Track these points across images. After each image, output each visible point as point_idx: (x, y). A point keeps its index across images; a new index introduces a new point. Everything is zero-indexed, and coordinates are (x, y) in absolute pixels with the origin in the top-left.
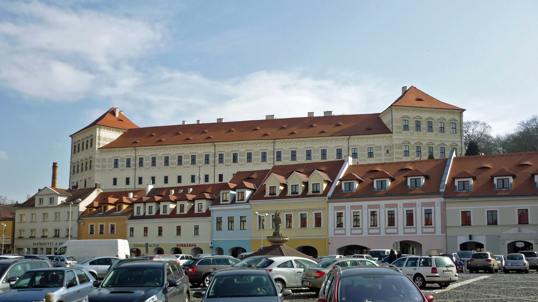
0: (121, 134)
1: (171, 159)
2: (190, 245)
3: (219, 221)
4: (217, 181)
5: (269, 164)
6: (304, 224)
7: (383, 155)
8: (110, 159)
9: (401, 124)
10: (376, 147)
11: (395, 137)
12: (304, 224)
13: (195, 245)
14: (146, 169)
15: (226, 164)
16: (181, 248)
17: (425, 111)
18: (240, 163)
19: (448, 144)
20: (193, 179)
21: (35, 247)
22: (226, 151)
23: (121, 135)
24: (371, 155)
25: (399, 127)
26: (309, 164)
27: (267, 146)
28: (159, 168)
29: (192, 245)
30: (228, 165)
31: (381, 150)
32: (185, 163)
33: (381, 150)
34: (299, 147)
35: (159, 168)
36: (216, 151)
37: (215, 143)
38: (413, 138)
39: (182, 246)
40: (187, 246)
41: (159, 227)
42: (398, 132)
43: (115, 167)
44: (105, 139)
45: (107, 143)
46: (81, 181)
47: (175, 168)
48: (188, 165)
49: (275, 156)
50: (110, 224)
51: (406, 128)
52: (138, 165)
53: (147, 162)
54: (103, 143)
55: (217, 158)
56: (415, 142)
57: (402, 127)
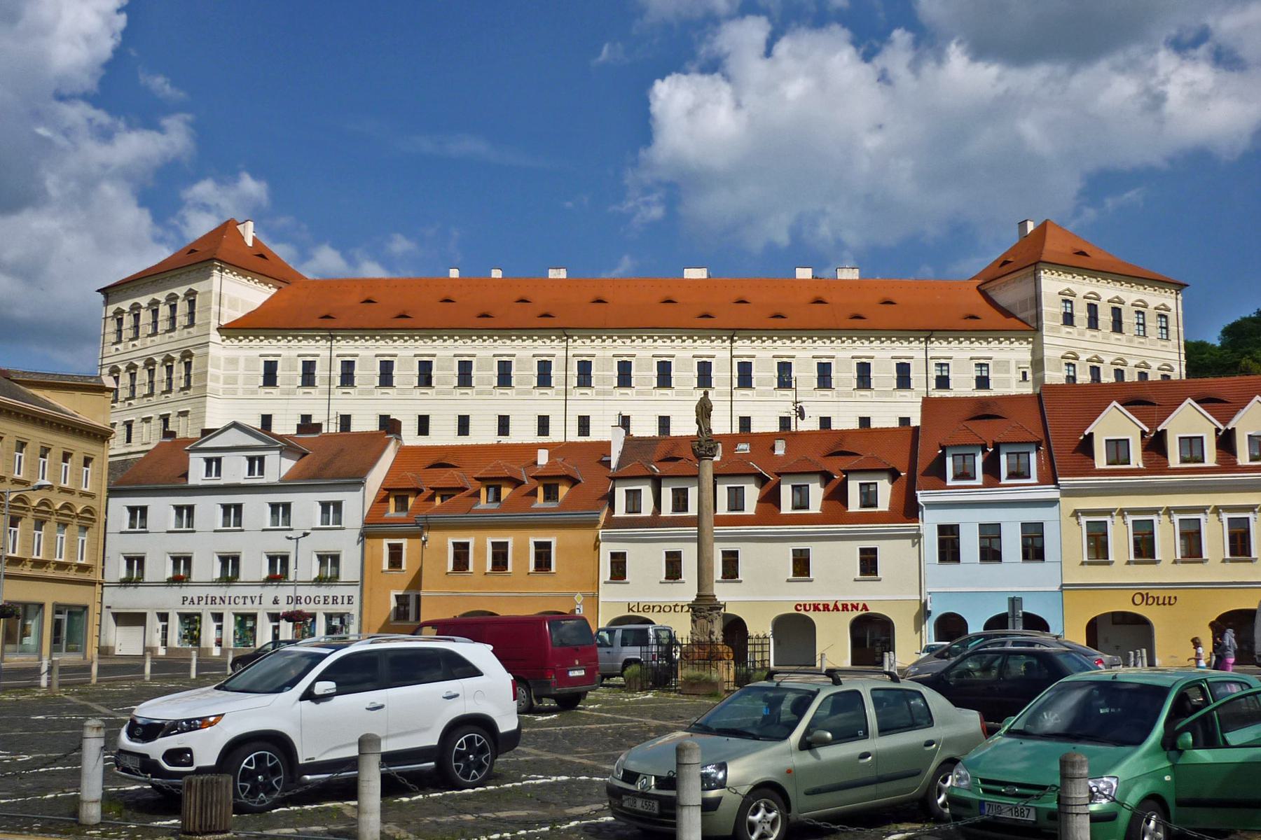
0: (274, 290)
2: (845, 607)
4: (573, 436)
7: (1014, 383)
8: (248, 360)
9: (1060, 310)
10: (997, 363)
11: (1046, 340)
13: (865, 607)
14: (639, 393)
16: (811, 614)
17: (1006, 284)
19: (1108, 359)
20: (543, 424)
21: (189, 609)
23: (273, 296)
24: (983, 382)
25: (1054, 316)
26: (941, 399)
28: (403, 391)
29: (855, 607)
30: (604, 393)
31: (1008, 371)
32: (481, 382)
33: (1008, 371)
34: (840, 354)
35: (403, 391)
36: (570, 353)
38: (1084, 345)
39: (816, 608)
42: (1052, 329)
44: (233, 305)
45: (239, 314)
46: (147, 420)
49: (736, 373)
50: (450, 542)
51: (1068, 319)
52: (338, 381)
54: (231, 315)
55: (574, 371)
56: (1089, 356)
57: (1061, 318)
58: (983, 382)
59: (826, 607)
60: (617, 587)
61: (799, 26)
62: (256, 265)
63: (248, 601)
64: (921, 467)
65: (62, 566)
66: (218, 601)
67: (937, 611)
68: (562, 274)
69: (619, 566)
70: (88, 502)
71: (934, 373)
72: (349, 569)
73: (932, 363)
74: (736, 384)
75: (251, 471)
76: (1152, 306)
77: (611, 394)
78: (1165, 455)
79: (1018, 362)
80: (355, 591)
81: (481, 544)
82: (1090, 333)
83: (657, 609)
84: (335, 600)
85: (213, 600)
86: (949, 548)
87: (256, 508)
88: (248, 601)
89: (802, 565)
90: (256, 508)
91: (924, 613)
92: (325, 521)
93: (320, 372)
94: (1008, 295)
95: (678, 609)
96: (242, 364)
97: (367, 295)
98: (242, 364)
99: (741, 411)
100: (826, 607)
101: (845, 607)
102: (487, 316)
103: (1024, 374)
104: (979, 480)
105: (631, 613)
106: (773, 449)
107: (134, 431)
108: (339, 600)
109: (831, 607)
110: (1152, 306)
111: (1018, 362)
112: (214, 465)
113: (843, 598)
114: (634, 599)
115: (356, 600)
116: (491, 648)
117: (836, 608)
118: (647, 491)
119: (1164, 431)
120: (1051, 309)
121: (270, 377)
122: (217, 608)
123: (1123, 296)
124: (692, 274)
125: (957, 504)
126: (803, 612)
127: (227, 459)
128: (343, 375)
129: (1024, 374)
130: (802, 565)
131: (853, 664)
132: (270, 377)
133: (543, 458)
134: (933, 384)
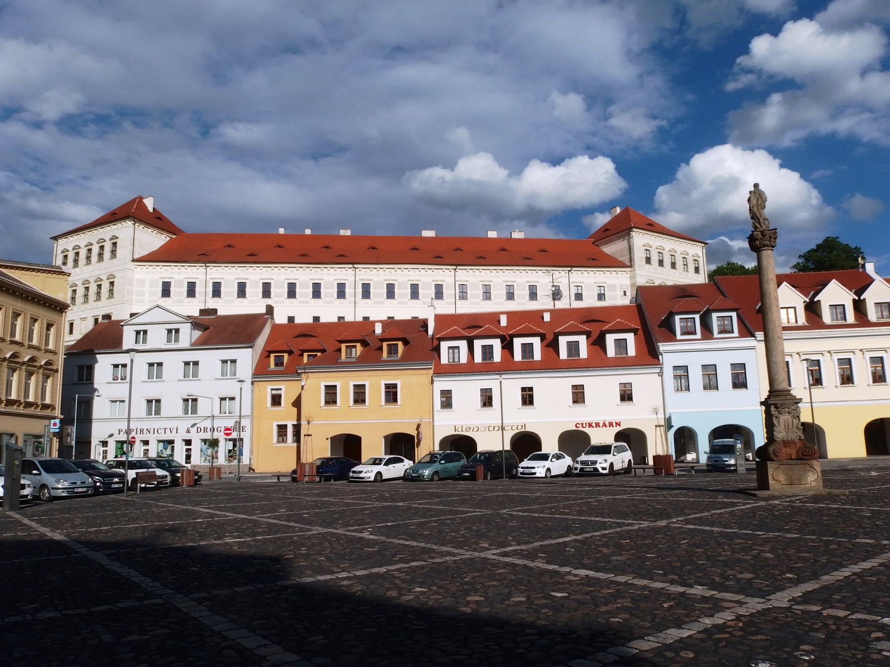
1: (276, 287)
2: (611, 424)
3: (682, 374)
5: (448, 303)
6: (847, 379)
7: (619, 298)
10: (609, 286)
11: (637, 272)
12: (847, 379)
15: (376, 300)
16: (587, 430)
18: (376, 300)
22: (176, 277)
24: (601, 297)
27: (445, 275)
30: (378, 303)
34: (375, 279)
37: (356, 266)
39: (590, 425)
40: (604, 425)
41: (523, 389)
43: (239, 297)
46: (83, 319)
47: (308, 302)
48: (308, 299)
49: (457, 291)
51: (648, 260)
53: (401, 291)
55: (359, 290)
58: (601, 297)
59: (597, 425)
60: (447, 412)
62: (156, 221)
63: (168, 431)
64: (653, 325)
65: (29, 405)
66: (145, 431)
67: (677, 424)
68: (348, 233)
69: (447, 400)
70: (50, 356)
71: (574, 291)
73: (572, 285)
74: (457, 297)
75: (169, 340)
76: (690, 255)
78: (820, 317)
79: (621, 285)
81: (345, 383)
82: (660, 268)
83: (476, 429)
85: (142, 431)
87: (173, 363)
88: (168, 431)
89: (578, 395)
90: (173, 363)
91: (669, 424)
92: (149, 412)
93: (348, 291)
94: (610, 249)
95: (491, 429)
96: (147, 283)
97: (227, 243)
98: (147, 283)
100: (597, 425)
101: (611, 424)
103: (625, 292)
104: (699, 335)
105: (457, 433)
106: (543, 318)
107: (75, 326)
109: (601, 425)
110: (690, 255)
111: (621, 285)
112: (142, 335)
113: (608, 419)
114: (459, 423)
117: (604, 425)
118: (463, 345)
119: (819, 301)
120: (639, 255)
121: (166, 291)
122: (145, 437)
123: (676, 248)
124: (426, 234)
125: (681, 352)
126: (581, 429)
128: (214, 291)
129: (625, 292)
130: (578, 395)
131: (870, 451)
132: (166, 291)
134: (573, 297)
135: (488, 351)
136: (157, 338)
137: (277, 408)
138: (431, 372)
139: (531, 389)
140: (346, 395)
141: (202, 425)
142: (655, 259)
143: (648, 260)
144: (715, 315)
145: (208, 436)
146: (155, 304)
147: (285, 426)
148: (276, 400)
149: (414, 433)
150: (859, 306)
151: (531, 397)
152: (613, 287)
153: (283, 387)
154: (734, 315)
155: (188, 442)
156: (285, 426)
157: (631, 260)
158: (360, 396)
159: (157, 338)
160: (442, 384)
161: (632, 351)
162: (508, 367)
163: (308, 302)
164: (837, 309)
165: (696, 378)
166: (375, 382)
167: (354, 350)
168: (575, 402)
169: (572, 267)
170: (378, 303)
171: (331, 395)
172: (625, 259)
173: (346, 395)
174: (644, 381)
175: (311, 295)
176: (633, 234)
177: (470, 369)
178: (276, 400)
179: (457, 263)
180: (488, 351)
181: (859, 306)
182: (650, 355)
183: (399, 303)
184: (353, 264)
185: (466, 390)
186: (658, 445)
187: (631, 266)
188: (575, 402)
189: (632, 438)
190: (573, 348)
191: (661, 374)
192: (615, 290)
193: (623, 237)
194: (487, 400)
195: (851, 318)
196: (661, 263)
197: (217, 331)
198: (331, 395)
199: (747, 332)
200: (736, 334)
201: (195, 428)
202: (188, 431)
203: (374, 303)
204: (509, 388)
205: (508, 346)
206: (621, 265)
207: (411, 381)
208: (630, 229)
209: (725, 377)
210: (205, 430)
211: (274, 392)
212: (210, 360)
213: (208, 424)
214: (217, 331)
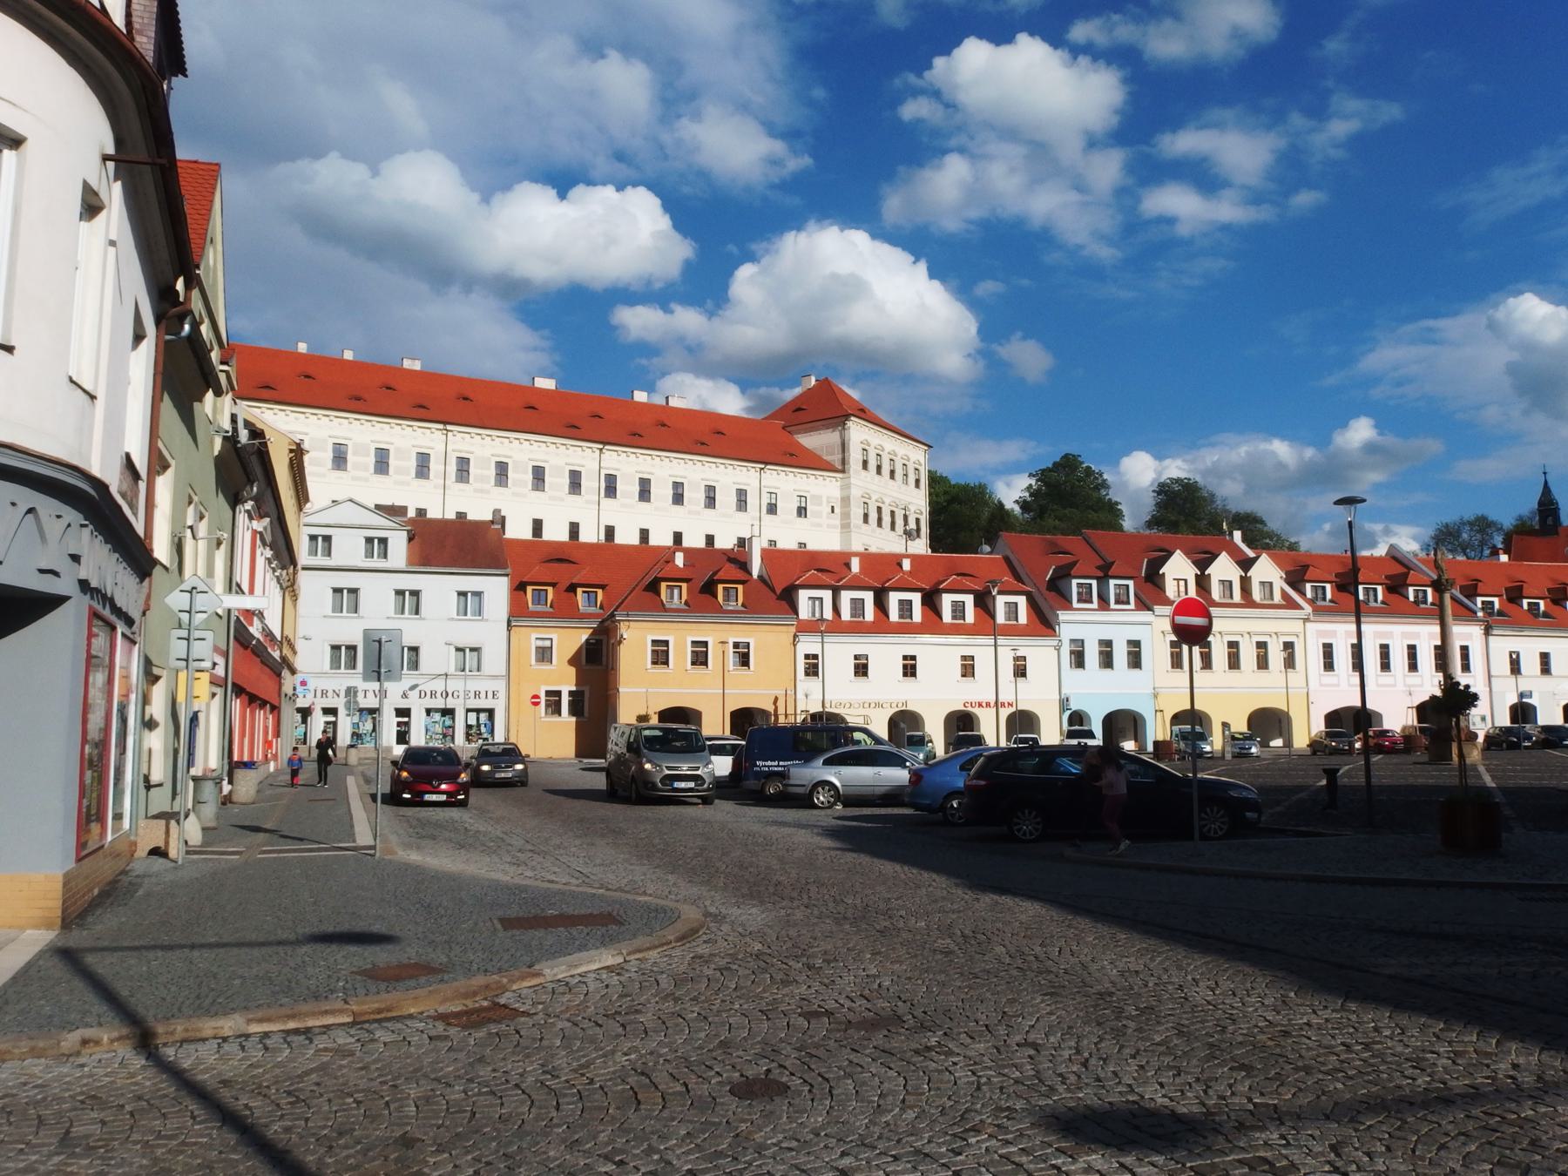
5: (588, 502)
9: (861, 458)
10: (813, 497)
19: (874, 498)
30: (482, 491)
39: (980, 705)
41: (964, 658)
49: (603, 485)
51: (865, 464)
55: (452, 468)
60: (1206, 673)
61: (1024, 338)
66: (330, 694)
67: (1074, 706)
68: (417, 366)
71: (765, 501)
72: (494, 660)
73: (764, 490)
77: (488, 492)
78: (1209, 593)
80: (500, 686)
81: (681, 637)
84: (477, 695)
85: (324, 693)
86: (1079, 660)
93: (435, 466)
94: (815, 441)
99: (606, 521)
102: (72, 381)
104: (1095, 605)
108: (483, 695)
115: (502, 695)
116: (1438, 693)
118: (827, 595)
120: (855, 457)
122: (330, 703)
127: (338, 537)
133: (679, 559)
135: (858, 605)
136: (349, 549)
137: (545, 667)
138: (793, 629)
139: (913, 658)
140: (680, 654)
141: (428, 687)
142: (872, 464)
143: (865, 464)
144: (1112, 582)
145: (439, 703)
146: (346, 497)
147: (558, 693)
148: (544, 654)
149: (771, 709)
150: (1245, 583)
151: (914, 667)
152: (818, 498)
153: (554, 636)
154: (1131, 583)
155: (403, 712)
156: (558, 693)
157: (844, 462)
158: (700, 659)
159: (349, 549)
160: (809, 645)
161: (1023, 618)
162: (881, 626)
163: (366, 480)
164: (1227, 585)
165: (1092, 655)
166: (719, 635)
167: (676, 592)
168: (1259, 667)
169: (767, 464)
170: (482, 491)
171: (661, 655)
172: (835, 459)
173: (680, 654)
174: (1041, 655)
175: (329, 464)
176: (849, 424)
177: (837, 627)
178: (544, 654)
179: (605, 440)
180: (858, 605)
181: (1245, 583)
182: (1044, 623)
183: (354, 479)
184: (445, 423)
185: (838, 653)
186: (993, 733)
187: (843, 471)
188: (1259, 667)
189: (1023, 721)
190: (958, 609)
191: (1058, 650)
192: (820, 504)
193: (834, 427)
194: (861, 669)
195: (1237, 597)
196: (879, 468)
197: (451, 545)
198: (661, 655)
199: (1144, 605)
200: (1132, 606)
201: (416, 691)
202: (405, 696)
203: (476, 491)
204: (885, 653)
205: (881, 605)
206: (827, 467)
207: (767, 638)
208: (847, 416)
209: (1120, 655)
210: (433, 694)
211: (540, 643)
212: (440, 588)
213: (438, 686)
214: (451, 545)
